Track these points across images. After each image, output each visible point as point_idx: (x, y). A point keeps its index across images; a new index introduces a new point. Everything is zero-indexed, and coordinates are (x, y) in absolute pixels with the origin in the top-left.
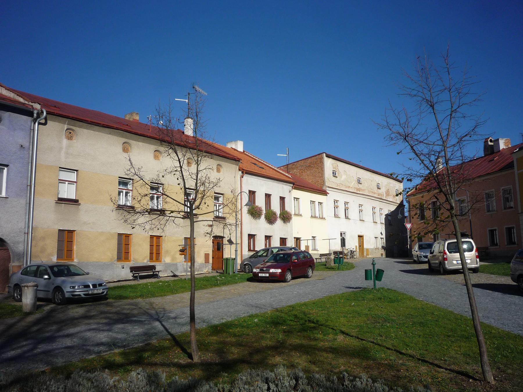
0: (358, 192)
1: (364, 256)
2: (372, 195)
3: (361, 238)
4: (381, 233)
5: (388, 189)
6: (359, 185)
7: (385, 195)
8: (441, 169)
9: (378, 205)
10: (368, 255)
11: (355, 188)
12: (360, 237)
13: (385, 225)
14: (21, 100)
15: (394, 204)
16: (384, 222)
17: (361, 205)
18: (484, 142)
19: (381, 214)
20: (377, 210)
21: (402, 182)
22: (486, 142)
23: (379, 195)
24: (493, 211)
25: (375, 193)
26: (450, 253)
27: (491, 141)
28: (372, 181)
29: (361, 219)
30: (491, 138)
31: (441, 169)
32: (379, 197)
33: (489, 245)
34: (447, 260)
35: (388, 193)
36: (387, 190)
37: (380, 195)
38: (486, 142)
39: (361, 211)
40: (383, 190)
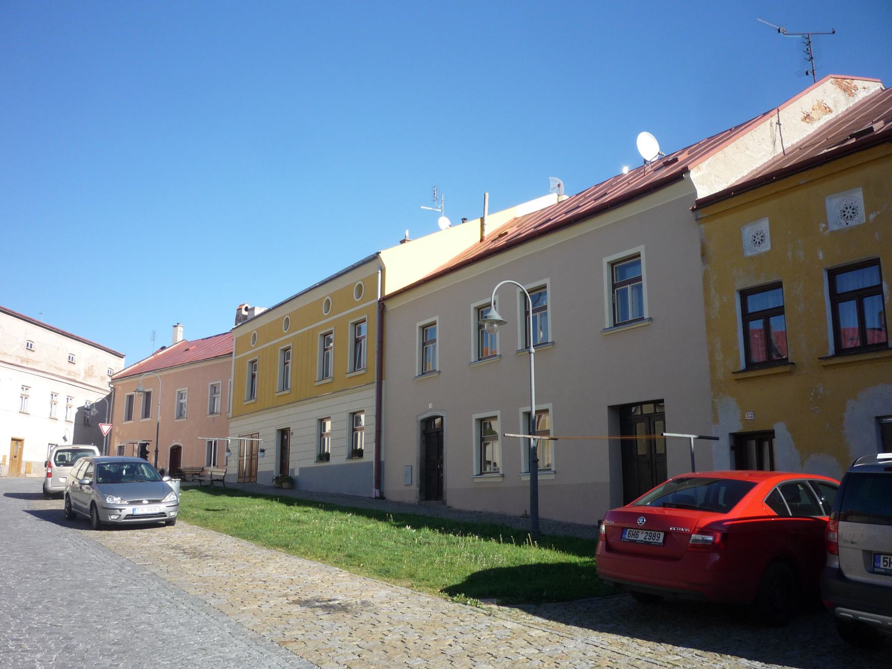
0: (24, 365)
1: (20, 474)
2: (53, 372)
3: (19, 443)
4: (65, 439)
5: (92, 366)
6: (29, 352)
7: (83, 375)
8: (179, 343)
9: (64, 390)
10: (29, 473)
11: (18, 357)
12: (17, 441)
13: (75, 424)
14: (837, 147)
15: (101, 391)
16: (73, 419)
17: (25, 388)
18: (238, 310)
19: (68, 407)
20: (61, 400)
21: (122, 358)
22: (240, 309)
23: (70, 373)
24: (217, 413)
25: (61, 370)
26: (58, 465)
27: (246, 309)
28: (58, 349)
29: (53, 416)
30: (246, 305)
31: (179, 343)
32: (69, 377)
33: (206, 465)
34: (51, 477)
35: (89, 372)
36: (89, 368)
37: (73, 374)
38: (240, 309)
39: (24, 397)
40: (80, 367)
